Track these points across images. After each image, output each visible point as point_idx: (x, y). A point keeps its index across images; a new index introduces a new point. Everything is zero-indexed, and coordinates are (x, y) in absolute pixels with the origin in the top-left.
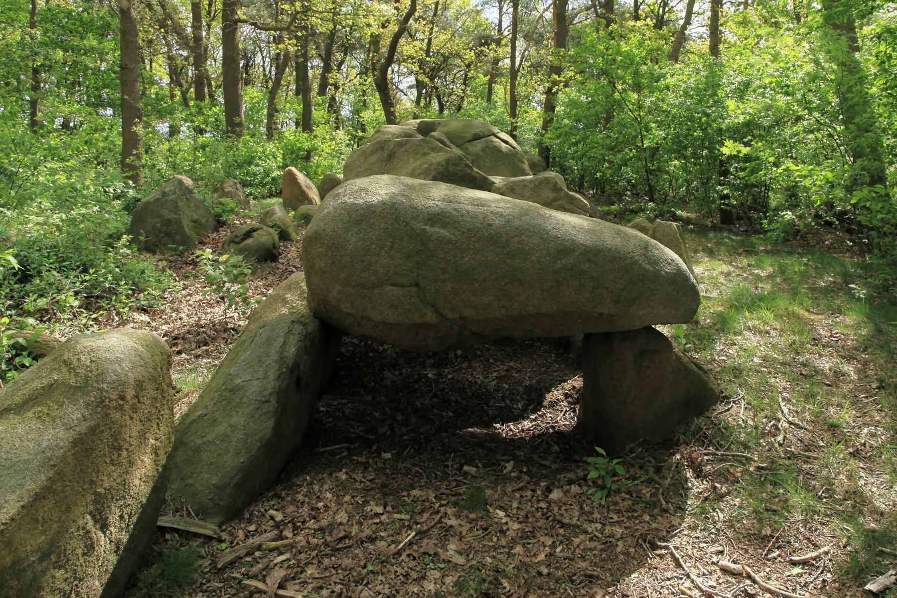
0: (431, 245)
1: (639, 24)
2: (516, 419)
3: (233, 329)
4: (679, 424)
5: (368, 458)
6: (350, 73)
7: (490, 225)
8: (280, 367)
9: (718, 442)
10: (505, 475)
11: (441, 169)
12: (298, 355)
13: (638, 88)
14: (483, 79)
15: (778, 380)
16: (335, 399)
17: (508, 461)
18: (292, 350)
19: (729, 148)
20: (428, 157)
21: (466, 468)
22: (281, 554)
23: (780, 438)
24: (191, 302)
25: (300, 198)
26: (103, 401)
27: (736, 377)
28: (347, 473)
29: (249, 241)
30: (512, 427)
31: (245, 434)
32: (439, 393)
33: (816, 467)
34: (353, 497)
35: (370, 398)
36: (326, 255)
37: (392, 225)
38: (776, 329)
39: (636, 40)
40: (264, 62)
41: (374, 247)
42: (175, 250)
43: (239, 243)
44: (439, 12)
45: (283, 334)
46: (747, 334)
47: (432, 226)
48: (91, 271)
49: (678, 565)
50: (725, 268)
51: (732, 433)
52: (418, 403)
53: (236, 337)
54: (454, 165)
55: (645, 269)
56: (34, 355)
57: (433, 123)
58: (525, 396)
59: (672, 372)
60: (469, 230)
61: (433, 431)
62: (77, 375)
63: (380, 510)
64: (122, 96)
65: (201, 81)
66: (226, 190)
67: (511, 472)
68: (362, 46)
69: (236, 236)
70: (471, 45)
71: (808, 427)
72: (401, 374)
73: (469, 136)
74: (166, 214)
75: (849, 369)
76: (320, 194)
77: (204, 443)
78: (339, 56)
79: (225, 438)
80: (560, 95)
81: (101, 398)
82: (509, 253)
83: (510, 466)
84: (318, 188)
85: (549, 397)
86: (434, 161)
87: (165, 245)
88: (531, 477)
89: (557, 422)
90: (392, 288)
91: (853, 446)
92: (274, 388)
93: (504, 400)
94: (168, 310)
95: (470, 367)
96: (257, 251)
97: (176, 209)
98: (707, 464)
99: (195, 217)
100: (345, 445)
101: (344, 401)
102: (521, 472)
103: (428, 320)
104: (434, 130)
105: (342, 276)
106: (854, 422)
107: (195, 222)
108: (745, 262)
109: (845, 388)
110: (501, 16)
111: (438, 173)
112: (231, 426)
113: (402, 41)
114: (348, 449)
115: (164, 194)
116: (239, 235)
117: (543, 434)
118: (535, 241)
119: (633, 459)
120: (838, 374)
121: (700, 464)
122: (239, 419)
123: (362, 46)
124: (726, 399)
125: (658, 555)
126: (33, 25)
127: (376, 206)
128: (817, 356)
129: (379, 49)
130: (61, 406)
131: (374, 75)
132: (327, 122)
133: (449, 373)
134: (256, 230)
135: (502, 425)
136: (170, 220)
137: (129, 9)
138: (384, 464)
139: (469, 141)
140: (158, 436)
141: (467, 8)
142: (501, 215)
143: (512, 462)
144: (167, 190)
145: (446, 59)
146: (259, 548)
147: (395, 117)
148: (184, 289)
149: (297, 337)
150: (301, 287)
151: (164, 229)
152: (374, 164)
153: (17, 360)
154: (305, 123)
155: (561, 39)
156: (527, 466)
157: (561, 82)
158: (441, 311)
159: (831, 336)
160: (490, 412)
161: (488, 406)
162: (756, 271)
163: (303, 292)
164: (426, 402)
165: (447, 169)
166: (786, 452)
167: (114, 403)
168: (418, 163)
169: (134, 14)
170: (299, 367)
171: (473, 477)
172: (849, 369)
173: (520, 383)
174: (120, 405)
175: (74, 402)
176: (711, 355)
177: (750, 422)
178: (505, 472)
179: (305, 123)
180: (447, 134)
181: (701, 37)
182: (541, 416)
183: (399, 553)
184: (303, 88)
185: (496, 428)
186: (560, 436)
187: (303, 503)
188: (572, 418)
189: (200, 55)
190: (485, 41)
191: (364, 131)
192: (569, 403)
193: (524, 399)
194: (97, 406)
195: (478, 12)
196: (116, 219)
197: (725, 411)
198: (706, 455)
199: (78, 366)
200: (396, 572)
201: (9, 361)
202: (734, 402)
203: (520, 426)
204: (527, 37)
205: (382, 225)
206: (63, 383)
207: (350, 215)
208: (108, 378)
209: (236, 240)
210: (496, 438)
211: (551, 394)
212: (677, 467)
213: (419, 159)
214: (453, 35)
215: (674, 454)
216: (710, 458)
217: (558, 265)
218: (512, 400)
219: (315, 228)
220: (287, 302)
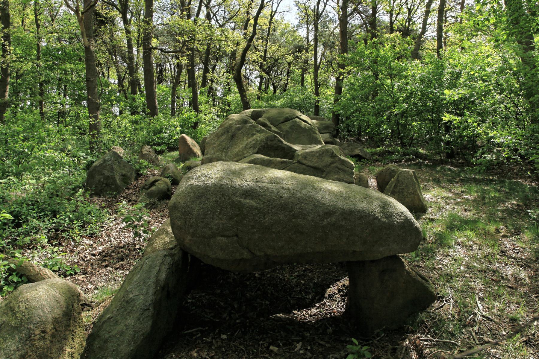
0: (245, 211)
1: (392, 36)
2: (308, 306)
3: (139, 249)
4: (409, 316)
5: (212, 339)
6: (221, 72)
7: (281, 197)
8: (156, 287)
9: (434, 331)
10: (296, 352)
12: (167, 279)
13: (391, 76)
14: (298, 72)
15: (476, 283)
16: (198, 293)
17: (298, 342)
18: (164, 275)
19: (446, 117)
20: (255, 137)
21: (271, 348)
23: (476, 328)
24: (118, 229)
26: (30, 337)
27: (448, 282)
28: (197, 352)
29: (153, 188)
30: (304, 312)
32: (261, 287)
33: (500, 351)
35: (219, 291)
37: (220, 199)
38: (476, 244)
39: (390, 45)
40: (171, 68)
42: (112, 194)
43: (147, 189)
44: (271, 33)
45: (158, 264)
46: (458, 248)
47: (245, 198)
48: (58, 216)
50: (446, 194)
51: (443, 324)
52: (248, 295)
53: (140, 254)
54: (271, 141)
55: (382, 222)
56: (20, 274)
57: (261, 111)
59: (404, 283)
60: (268, 201)
61: (255, 317)
62: (16, 318)
65: (134, 83)
66: (144, 153)
67: (300, 350)
68: (227, 56)
69: (146, 185)
70: (290, 52)
71: (496, 320)
73: (282, 119)
74: (106, 173)
75: (524, 274)
76: (201, 149)
77: (110, 337)
78: (213, 62)
79: (122, 333)
80: (345, 80)
81: (29, 334)
82: (293, 215)
83: (299, 346)
85: (329, 291)
87: (106, 191)
88: (312, 354)
89: (333, 309)
90: (221, 238)
91: (526, 336)
92: (152, 300)
93: (301, 293)
94: (104, 235)
95: (282, 268)
96: (158, 194)
97: (112, 169)
98: (426, 348)
99: (124, 173)
100: (200, 328)
101: (203, 294)
102: (306, 349)
103: (245, 257)
104: (261, 117)
105: (191, 231)
106: (527, 316)
107: (123, 176)
108: (460, 189)
109: (522, 290)
110: (308, 33)
111: (261, 146)
112: (126, 325)
113: (249, 52)
114: (201, 332)
115: (105, 161)
116: (148, 184)
117: (323, 319)
118: (310, 207)
119: (378, 341)
120: (518, 280)
121: (421, 348)
122: (131, 321)
123: (227, 56)
124: (441, 298)
126: (38, 59)
127: (211, 187)
128: (503, 265)
129: (236, 58)
130: (5, 340)
131: (233, 74)
132: (207, 102)
133: (268, 273)
135: (299, 311)
136: (108, 176)
137: (89, 46)
138: (222, 343)
139: (282, 123)
140: (73, 346)
141: (288, 29)
142: (289, 190)
143: (301, 343)
144: (106, 158)
145: (276, 60)
147: (247, 98)
148: (115, 220)
149: (167, 266)
152: (223, 141)
153: (10, 278)
154: (194, 104)
155: (344, 49)
156: (310, 345)
157: (345, 73)
158: (253, 251)
159: (514, 249)
160: (292, 302)
161: (291, 297)
162: (466, 197)
165: (267, 144)
166: (480, 339)
167: (38, 337)
168: (250, 140)
169: (92, 49)
170: (168, 285)
171: (276, 354)
172: (524, 274)
173: (311, 280)
174: (42, 336)
175: (13, 338)
176: (433, 264)
177: (456, 316)
178: (296, 350)
179: (194, 104)
180: (269, 119)
181: (433, 39)
182: (323, 304)
184: (192, 84)
185: (294, 314)
186: (332, 321)
188: (343, 306)
189: (132, 70)
190: (299, 49)
191: (229, 106)
192: (341, 295)
193: (313, 292)
194: (26, 340)
195: (295, 31)
196: (81, 176)
197: (440, 308)
198: (427, 340)
199: (18, 312)
201: (6, 279)
202: (446, 301)
203: (309, 312)
204: (325, 45)
205: (214, 199)
206: (8, 324)
207: (195, 193)
208: (34, 320)
210: (292, 322)
211: (330, 289)
212: (406, 350)
213: (249, 138)
214: (280, 46)
215: (404, 339)
216: (429, 343)
218: (306, 292)
219: (175, 201)
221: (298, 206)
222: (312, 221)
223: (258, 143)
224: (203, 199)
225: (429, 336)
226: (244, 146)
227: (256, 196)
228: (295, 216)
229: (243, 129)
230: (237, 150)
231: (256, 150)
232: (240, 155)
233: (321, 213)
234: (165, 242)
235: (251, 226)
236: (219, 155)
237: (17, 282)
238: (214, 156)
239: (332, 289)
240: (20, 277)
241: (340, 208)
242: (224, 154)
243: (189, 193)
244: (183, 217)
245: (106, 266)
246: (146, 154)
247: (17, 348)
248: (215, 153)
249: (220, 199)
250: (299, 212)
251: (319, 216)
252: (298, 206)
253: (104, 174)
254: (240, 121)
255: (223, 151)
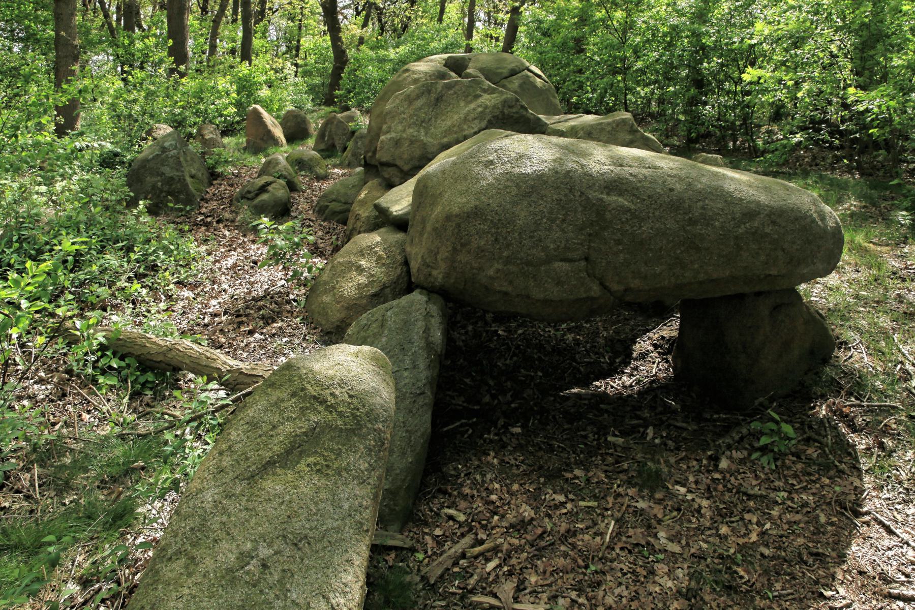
0: (608, 216)
3: (295, 301)
7: (671, 190)
11: (497, 112)
18: (437, 335)
20: (481, 100)
22: (488, 560)
25: (265, 138)
29: (265, 197)
31: (407, 431)
34: (521, 485)
36: (488, 232)
37: (566, 195)
41: (545, 220)
43: (252, 199)
49: (890, 532)
56: (119, 355)
58: (608, 348)
60: (649, 197)
62: (341, 414)
63: (562, 498)
64: (57, 34)
67: (654, 438)
69: (249, 192)
72: (466, 333)
73: (505, 72)
74: (168, 171)
82: (690, 219)
84: (281, 124)
86: (488, 103)
90: (561, 264)
92: (427, 378)
96: (273, 207)
100: (464, 421)
102: (662, 437)
111: (494, 117)
116: (251, 189)
118: (719, 205)
125: (864, 523)
134: (271, 183)
136: (172, 178)
139: (506, 78)
146: (463, 556)
147: (342, 43)
150: (376, 253)
151: (166, 188)
152: (420, 109)
153: (103, 361)
163: (380, 258)
164: (508, 362)
165: (502, 112)
168: (472, 106)
175: (353, 449)
178: (648, 438)
180: (482, 70)
183: (611, 548)
186: (652, 391)
187: (473, 496)
192: (659, 353)
200: (622, 569)
205: (555, 197)
209: (249, 196)
213: (470, 102)
217: (741, 230)
220: (363, 270)
221: (701, 203)
222: (722, 228)
223: (488, 110)
224: (534, 197)
225: (853, 399)
226: (462, 116)
227: (626, 190)
228: (692, 222)
229: (457, 87)
230: (449, 123)
231: (483, 124)
232: (456, 133)
233: (738, 215)
234: (359, 285)
235: (615, 240)
236: (415, 134)
237: (119, 367)
238: (404, 135)
239: (642, 345)
240: (122, 358)
241: (767, 206)
242: (422, 131)
243: (506, 187)
244: (493, 230)
245: (251, 333)
246: (211, 139)
247: (370, 465)
248: (404, 131)
249: (566, 195)
250: (701, 214)
251: (734, 219)
252: (701, 203)
253: (163, 174)
254: (434, 74)
255: (421, 125)
